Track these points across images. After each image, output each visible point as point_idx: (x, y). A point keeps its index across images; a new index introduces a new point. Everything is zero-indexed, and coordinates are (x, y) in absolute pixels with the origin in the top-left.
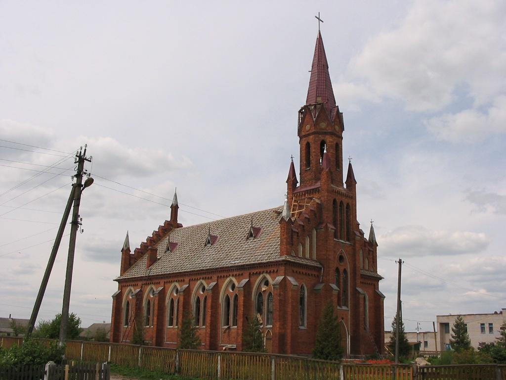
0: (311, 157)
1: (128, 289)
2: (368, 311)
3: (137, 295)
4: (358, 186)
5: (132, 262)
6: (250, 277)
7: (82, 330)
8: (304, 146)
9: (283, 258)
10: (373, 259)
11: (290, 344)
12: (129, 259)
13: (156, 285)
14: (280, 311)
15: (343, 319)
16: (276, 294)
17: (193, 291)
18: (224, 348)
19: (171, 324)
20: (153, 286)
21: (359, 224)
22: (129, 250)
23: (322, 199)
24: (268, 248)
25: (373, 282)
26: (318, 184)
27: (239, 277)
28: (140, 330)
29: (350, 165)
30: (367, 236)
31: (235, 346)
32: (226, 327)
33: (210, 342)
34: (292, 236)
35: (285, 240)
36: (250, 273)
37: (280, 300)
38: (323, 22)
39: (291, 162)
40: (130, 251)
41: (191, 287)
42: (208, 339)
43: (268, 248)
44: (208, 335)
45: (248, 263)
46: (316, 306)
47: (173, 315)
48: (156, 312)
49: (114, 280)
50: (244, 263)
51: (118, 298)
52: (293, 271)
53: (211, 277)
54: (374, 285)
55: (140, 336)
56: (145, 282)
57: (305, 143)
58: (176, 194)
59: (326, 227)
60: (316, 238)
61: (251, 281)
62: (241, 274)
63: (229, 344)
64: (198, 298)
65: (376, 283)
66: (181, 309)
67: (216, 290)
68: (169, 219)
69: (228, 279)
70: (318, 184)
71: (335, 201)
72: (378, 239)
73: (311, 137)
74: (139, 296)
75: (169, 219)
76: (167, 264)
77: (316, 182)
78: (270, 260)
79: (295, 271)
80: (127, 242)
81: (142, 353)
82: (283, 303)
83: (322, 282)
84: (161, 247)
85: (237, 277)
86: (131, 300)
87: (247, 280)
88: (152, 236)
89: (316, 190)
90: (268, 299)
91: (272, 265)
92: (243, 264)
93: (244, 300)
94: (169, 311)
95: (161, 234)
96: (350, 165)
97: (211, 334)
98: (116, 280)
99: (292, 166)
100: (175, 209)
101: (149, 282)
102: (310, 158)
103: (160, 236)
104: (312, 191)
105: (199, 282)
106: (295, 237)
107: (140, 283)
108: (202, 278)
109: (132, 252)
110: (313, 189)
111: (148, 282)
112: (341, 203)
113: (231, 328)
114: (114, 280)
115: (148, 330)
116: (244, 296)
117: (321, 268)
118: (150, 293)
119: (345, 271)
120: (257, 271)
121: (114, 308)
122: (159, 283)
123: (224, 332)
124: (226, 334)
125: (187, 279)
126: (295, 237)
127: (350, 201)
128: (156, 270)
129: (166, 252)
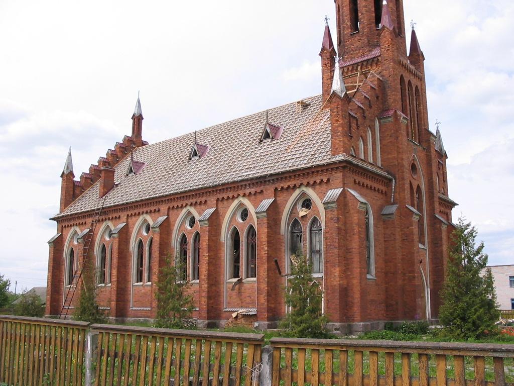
0: (359, 14)
1: (72, 230)
3: (84, 237)
5: (77, 192)
6: (275, 196)
7: (16, 297)
9: (340, 157)
11: (359, 304)
12: (72, 189)
13: (114, 221)
14: (340, 247)
16: (332, 219)
17: (174, 225)
18: (234, 315)
19: (140, 278)
20: (110, 223)
22: (71, 174)
23: (384, 73)
24: (314, 143)
26: (376, 52)
27: (255, 196)
28: (90, 290)
29: (413, 33)
31: (253, 311)
32: (235, 280)
33: (208, 304)
34: (350, 122)
35: (340, 129)
36: (276, 189)
37: (339, 229)
39: (324, 25)
40: (74, 177)
41: (172, 219)
42: (204, 301)
43: (314, 143)
44: (204, 294)
45: (272, 172)
46: (385, 241)
47: (142, 266)
48: (115, 261)
49: (50, 219)
50: (265, 173)
51: (56, 245)
52: (355, 181)
53: (206, 201)
54: (447, 213)
55: (91, 298)
56: (96, 218)
58: (139, 99)
59: (395, 115)
61: (279, 202)
62: (118, 216)
63: (242, 307)
64: (184, 236)
65: (448, 211)
66: (156, 254)
67: (215, 220)
68: (130, 134)
69: (236, 202)
70: (376, 52)
71: (402, 78)
74: (88, 241)
75: (130, 134)
76: (129, 189)
77: (370, 51)
78: (314, 164)
80: (69, 164)
81: (99, 353)
82: (343, 232)
83: (393, 204)
84: (121, 170)
86: (76, 247)
87: (271, 200)
88: (106, 157)
89: (374, 61)
90: (311, 231)
91: (318, 172)
92: (262, 174)
93: (268, 232)
94: (136, 259)
95: (119, 154)
96: (413, 33)
97: (208, 292)
98: (53, 219)
99: (327, 30)
100: (138, 120)
101: (104, 217)
103: (117, 157)
104: (365, 63)
105: (184, 210)
106: (354, 125)
107: (89, 221)
108: (189, 203)
109: (77, 178)
110: (367, 61)
111: (101, 218)
112: (409, 82)
113: (243, 281)
114: (50, 219)
115: (102, 290)
116: (269, 227)
117: (391, 180)
118: (105, 234)
119: (419, 187)
120: (289, 183)
121: (51, 260)
122: (119, 217)
123: (233, 289)
124: (235, 293)
125: (164, 208)
126: (354, 125)
127: (419, 84)
128: (114, 199)
129: (127, 175)
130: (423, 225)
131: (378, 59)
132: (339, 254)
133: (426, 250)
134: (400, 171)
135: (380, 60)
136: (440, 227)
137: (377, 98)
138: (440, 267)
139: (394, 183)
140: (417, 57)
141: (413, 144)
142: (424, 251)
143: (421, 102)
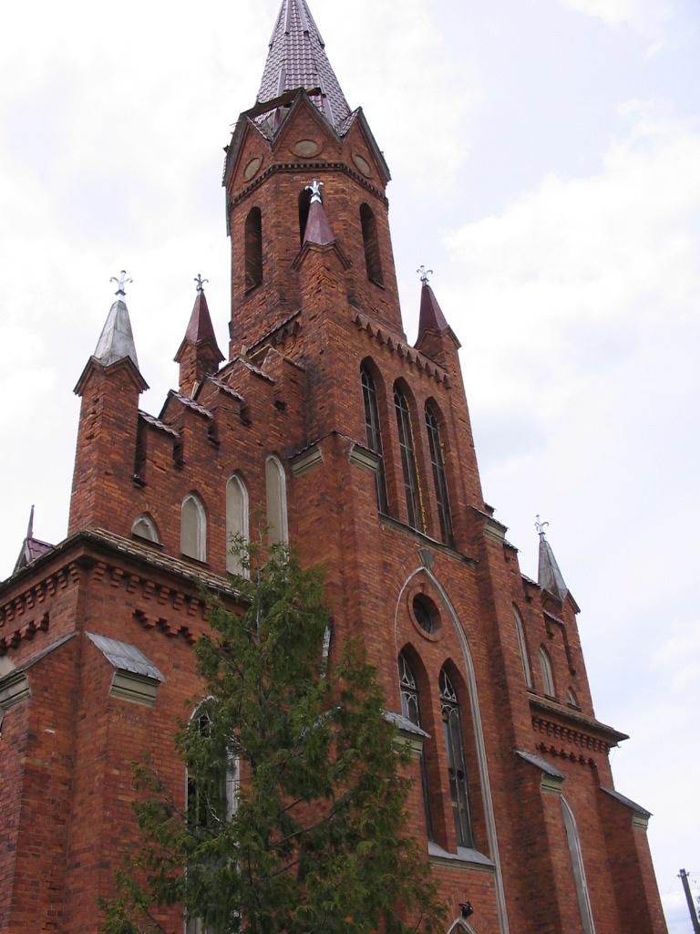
0: (265, 245)
2: (584, 883)
4: (468, 360)
8: (241, 229)
10: (569, 660)
15: (466, 912)
25: (587, 754)
29: (427, 293)
30: (529, 567)
37: (33, 778)
54: (591, 763)
57: (242, 216)
60: (290, 494)
65: (596, 757)
71: (368, 368)
72: (574, 581)
96: (427, 293)
102: (260, 249)
119: (450, 669)
120: (28, 617)
130: (479, 789)
131: (297, 324)
132: (18, 875)
133: (492, 868)
134: (351, 603)
135: (300, 324)
136: (536, 788)
137: (280, 405)
138: (552, 928)
139: (327, 637)
140: (436, 339)
141: (418, 540)
142: (486, 873)
143: (451, 440)
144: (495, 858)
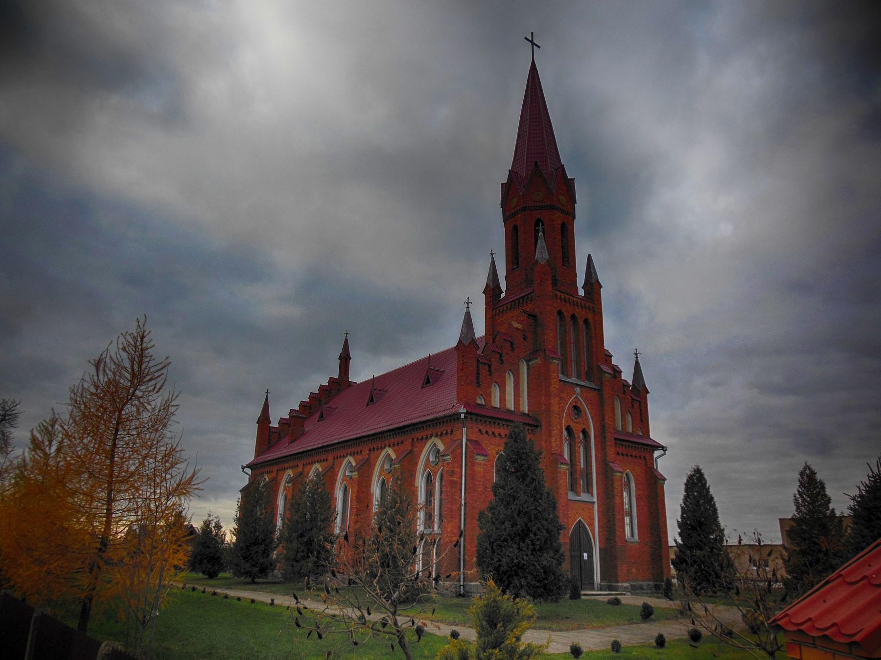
21: (611, 356)
30: (627, 376)
38: (526, 38)
68: (336, 376)
73: (519, 215)
75: (336, 376)
79: (484, 431)
85: (396, 447)
100: (345, 360)
109: (274, 424)
127: (590, 316)
144: (595, 500)
